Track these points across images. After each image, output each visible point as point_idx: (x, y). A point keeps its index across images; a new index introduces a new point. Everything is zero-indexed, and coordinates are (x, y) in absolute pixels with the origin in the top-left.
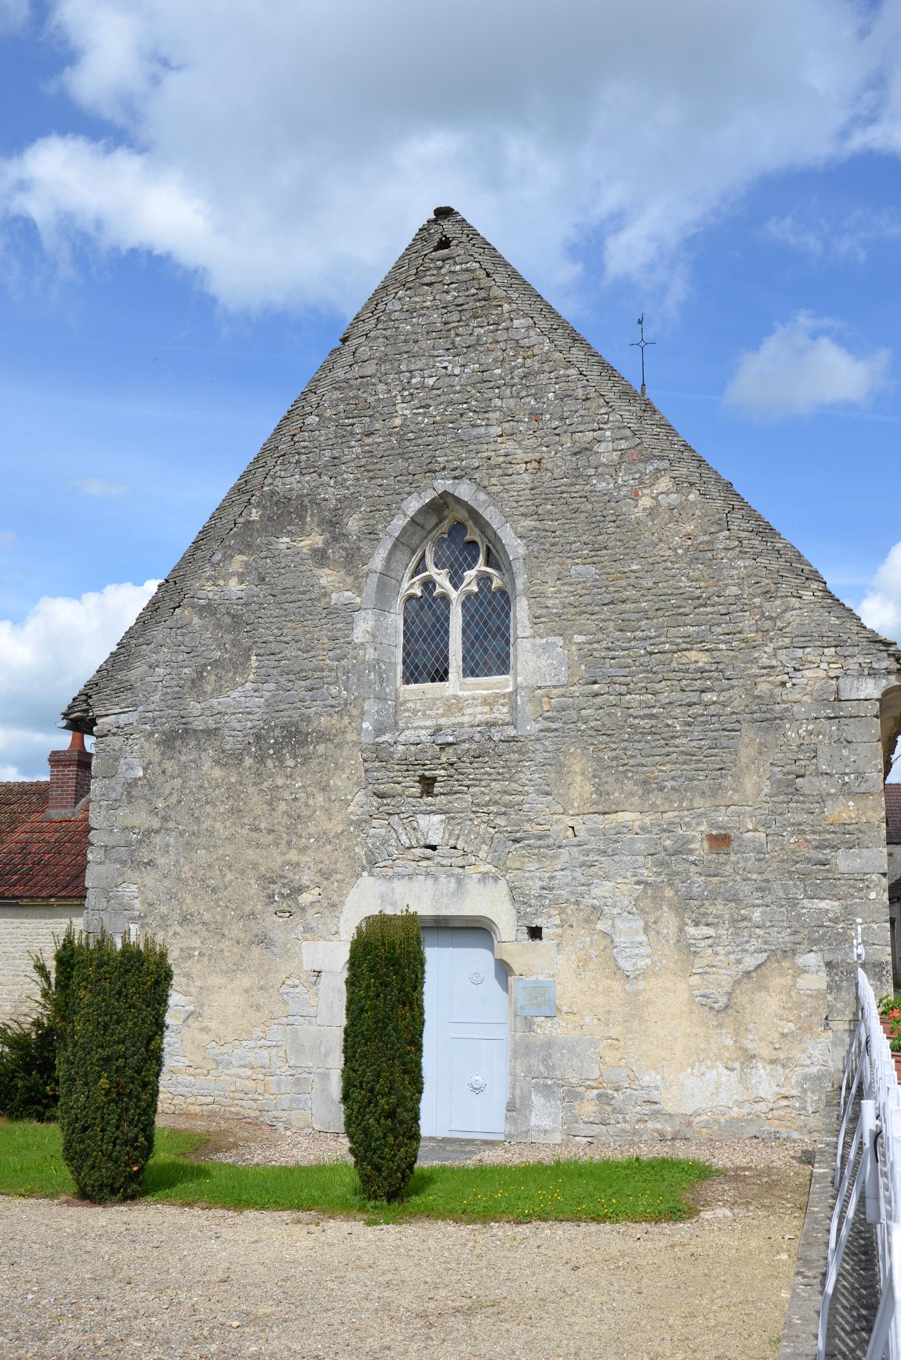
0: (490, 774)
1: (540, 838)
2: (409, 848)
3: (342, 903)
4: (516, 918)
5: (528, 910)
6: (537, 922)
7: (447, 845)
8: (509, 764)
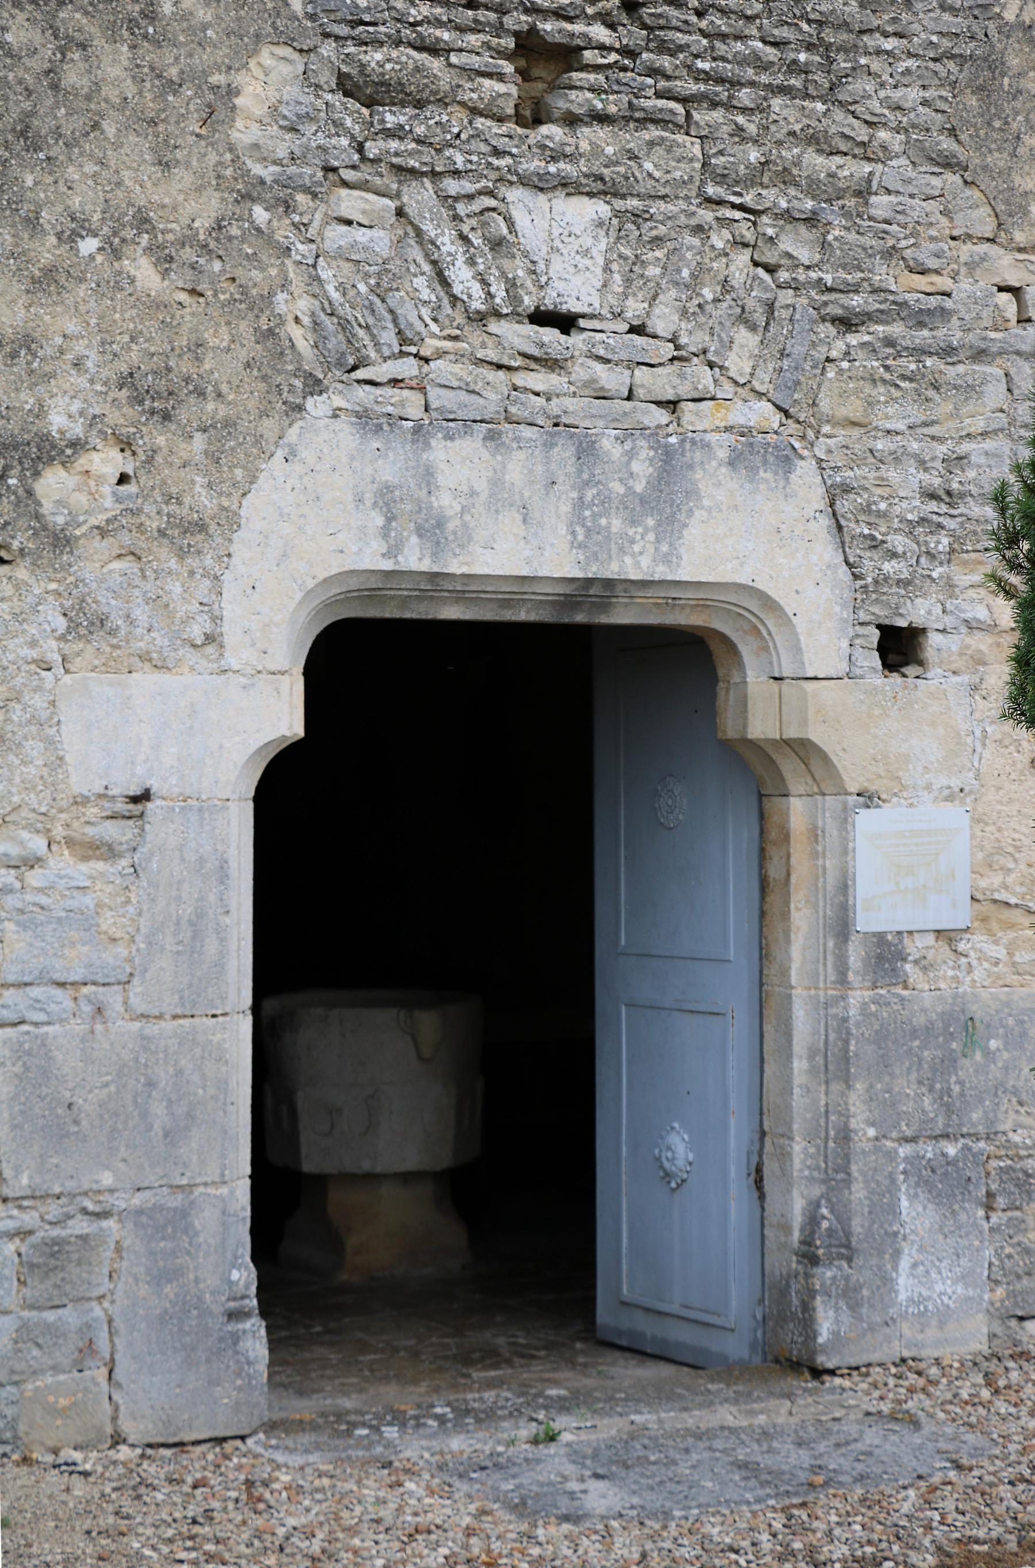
0: (764, 66)
1: (921, 319)
2: (480, 319)
3: (231, 521)
4: (848, 595)
5: (888, 567)
6: (918, 611)
7: (618, 315)
8: (829, 36)
